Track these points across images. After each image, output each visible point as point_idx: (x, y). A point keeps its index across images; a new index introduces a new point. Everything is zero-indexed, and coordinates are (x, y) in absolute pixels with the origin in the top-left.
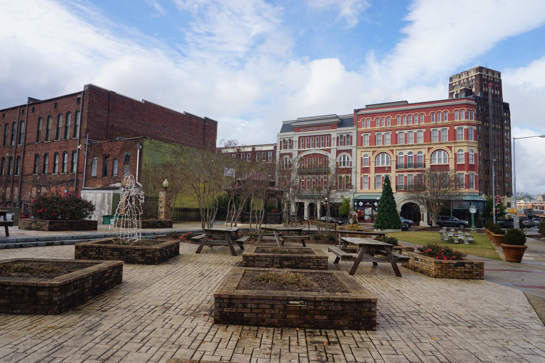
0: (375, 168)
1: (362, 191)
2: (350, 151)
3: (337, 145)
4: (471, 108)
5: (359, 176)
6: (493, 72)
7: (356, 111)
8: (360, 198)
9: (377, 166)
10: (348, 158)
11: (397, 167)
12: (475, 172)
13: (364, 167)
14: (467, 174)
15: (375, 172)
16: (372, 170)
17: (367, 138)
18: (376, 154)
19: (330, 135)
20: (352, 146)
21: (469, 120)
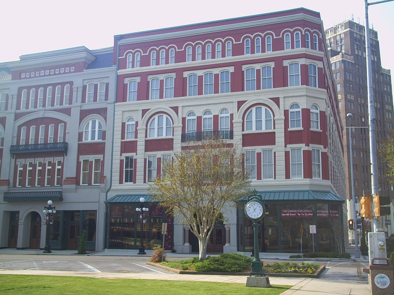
2: (102, 112)
3: (83, 101)
7: (118, 38)
11: (184, 138)
12: (322, 146)
13: (126, 140)
14: (306, 148)
16: (141, 146)
19: (71, 83)
20: (108, 101)
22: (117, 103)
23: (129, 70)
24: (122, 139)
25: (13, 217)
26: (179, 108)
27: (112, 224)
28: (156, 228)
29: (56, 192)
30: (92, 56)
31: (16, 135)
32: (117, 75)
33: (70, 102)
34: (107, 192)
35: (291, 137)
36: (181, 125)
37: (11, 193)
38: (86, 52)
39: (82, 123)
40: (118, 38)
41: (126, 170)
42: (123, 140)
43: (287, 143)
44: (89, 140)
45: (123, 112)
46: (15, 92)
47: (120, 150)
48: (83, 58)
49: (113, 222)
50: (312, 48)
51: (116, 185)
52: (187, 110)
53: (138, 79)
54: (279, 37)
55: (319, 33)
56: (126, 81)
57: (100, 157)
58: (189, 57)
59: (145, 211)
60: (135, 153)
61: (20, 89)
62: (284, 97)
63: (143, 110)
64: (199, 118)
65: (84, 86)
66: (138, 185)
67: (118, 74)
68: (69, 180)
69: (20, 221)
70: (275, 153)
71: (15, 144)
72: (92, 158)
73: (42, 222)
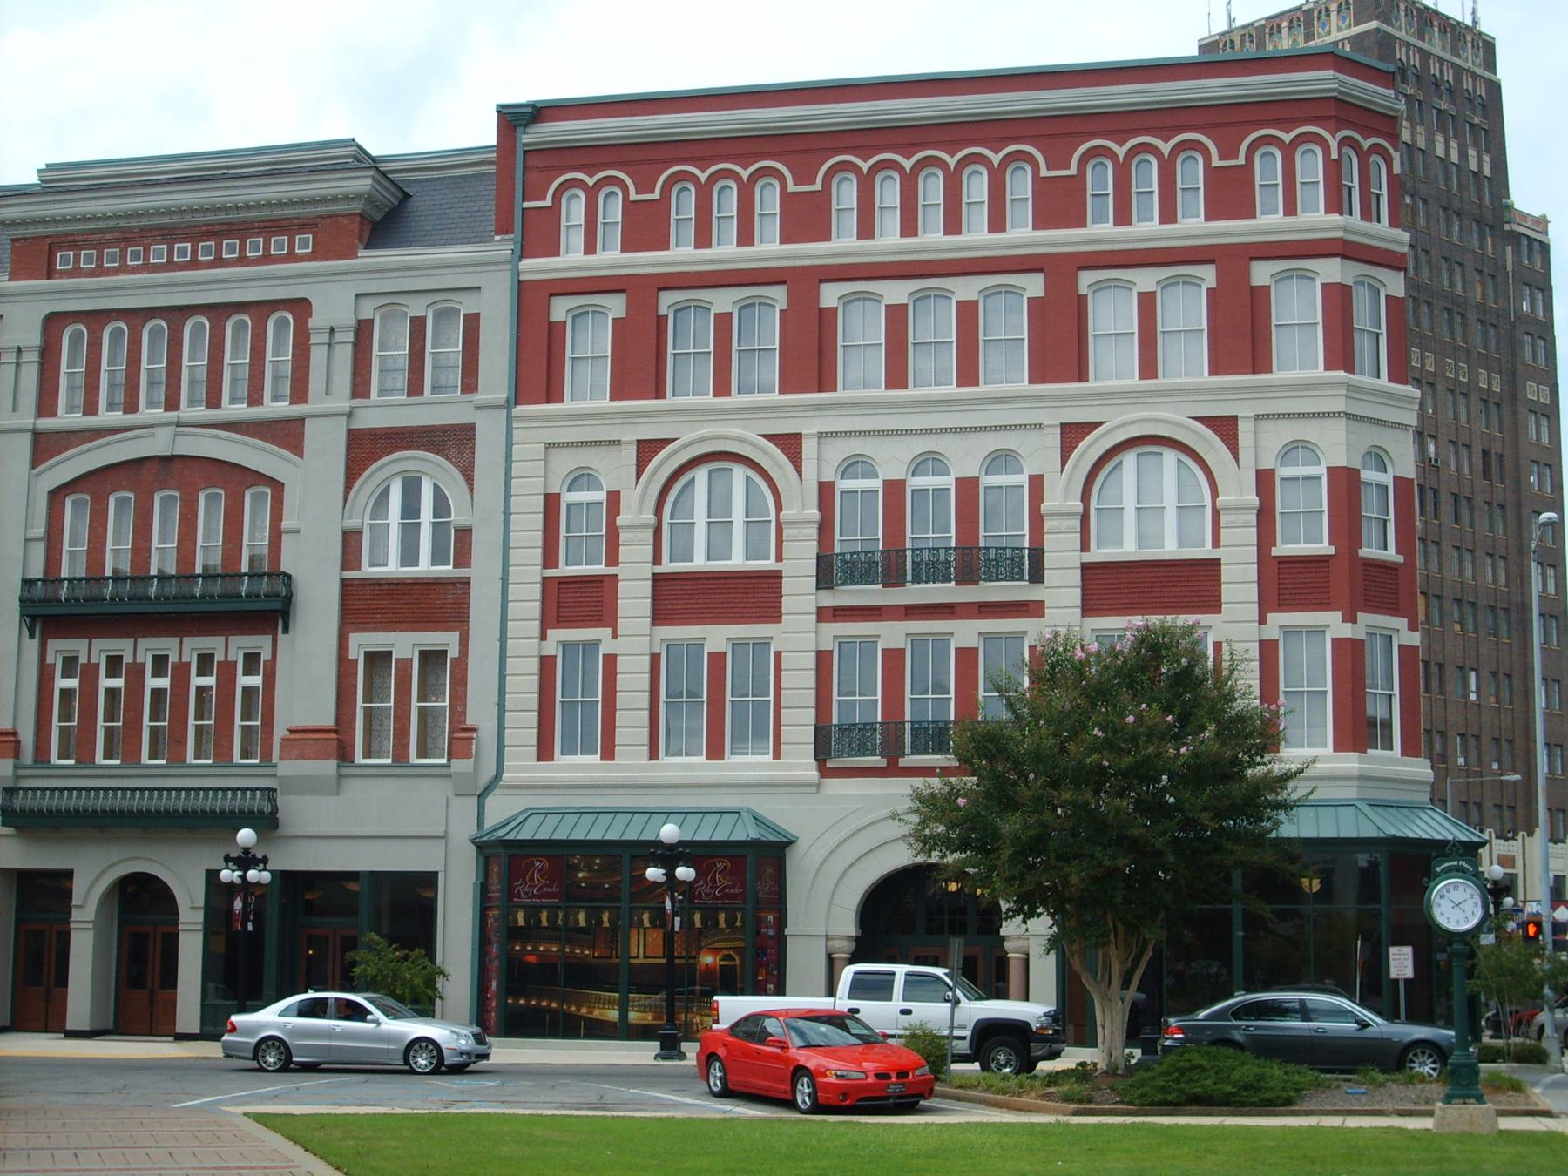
0: (658, 579)
1: (544, 773)
2: (453, 442)
3: (360, 388)
4: (1367, 132)
5: (528, 643)
6: (1456, 33)
7: (513, 119)
8: (525, 834)
9: (668, 566)
10: (439, 495)
12: (1401, 623)
13: (565, 570)
14: (1347, 631)
15: (658, 618)
16: (634, 599)
17: (591, 343)
18: (663, 465)
19: (301, 307)
20: (478, 398)
21: (1355, 220)
22: (519, 408)
23: (571, 259)
24: (545, 566)
25: (44, 894)
26: (1240, 423)
27: (514, 934)
28: (715, 951)
29: (253, 790)
30: (388, 185)
31: (39, 530)
32: (521, 285)
33: (299, 393)
34: (482, 796)
35: (1287, 583)
36: (814, 513)
37: (26, 790)
38: (371, 173)
39: (356, 487)
40: (513, 119)
41: (420, 708)
42: (551, 573)
43: (1266, 605)
44: (392, 567)
45: (549, 445)
46: (33, 338)
47: (537, 614)
48: (357, 197)
49: (521, 923)
50: (1366, 215)
51: (522, 766)
52: (839, 451)
53: (616, 306)
54: (1233, 163)
55: (1392, 150)
56: (560, 309)
57: (448, 640)
58: (574, 240)
59: (258, 884)
60: (609, 630)
61: (54, 323)
62: (1257, 417)
63: (639, 442)
64: (894, 489)
65: (359, 322)
66: (624, 768)
67: (523, 278)
68: (304, 740)
69: (76, 915)
70: (778, 655)
71: (37, 571)
72: (405, 644)
73: (182, 919)
